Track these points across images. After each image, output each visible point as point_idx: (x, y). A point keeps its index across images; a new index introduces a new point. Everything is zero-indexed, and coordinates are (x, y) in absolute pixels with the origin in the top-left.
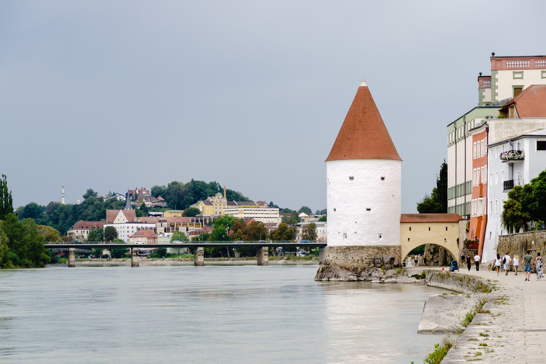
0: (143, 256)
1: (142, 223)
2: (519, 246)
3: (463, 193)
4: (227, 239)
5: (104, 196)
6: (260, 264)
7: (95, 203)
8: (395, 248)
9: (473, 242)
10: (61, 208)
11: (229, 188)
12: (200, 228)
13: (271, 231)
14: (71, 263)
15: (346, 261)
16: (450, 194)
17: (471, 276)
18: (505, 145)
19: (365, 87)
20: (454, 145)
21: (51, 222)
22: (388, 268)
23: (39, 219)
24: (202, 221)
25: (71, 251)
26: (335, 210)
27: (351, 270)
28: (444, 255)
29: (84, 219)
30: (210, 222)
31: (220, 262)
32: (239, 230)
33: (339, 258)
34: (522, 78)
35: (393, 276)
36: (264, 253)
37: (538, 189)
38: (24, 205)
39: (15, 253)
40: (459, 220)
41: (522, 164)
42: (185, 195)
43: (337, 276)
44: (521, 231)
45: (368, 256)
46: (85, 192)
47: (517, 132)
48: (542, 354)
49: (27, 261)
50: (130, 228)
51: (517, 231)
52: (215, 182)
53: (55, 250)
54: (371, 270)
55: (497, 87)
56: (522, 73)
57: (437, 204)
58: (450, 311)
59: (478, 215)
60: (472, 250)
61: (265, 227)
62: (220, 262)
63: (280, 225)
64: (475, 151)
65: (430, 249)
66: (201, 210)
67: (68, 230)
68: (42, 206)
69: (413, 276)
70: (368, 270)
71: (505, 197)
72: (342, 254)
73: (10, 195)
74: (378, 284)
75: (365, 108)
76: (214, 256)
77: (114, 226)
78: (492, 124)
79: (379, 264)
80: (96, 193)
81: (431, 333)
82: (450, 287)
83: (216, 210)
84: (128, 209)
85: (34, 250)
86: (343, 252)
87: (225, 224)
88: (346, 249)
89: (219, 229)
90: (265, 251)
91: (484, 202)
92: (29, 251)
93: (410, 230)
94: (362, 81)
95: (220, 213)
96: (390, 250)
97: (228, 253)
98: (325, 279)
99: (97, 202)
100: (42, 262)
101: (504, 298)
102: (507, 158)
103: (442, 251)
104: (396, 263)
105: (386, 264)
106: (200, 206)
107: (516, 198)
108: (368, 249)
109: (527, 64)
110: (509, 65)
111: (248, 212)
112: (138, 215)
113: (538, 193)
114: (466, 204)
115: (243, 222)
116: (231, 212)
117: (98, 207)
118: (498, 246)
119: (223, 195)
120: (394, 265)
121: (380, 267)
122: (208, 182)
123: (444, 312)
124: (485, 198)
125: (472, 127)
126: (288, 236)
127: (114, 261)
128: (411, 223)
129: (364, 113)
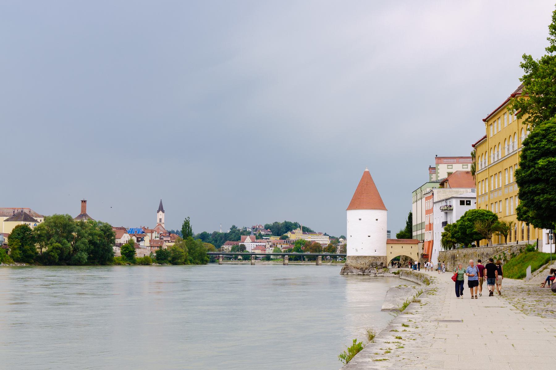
0: (258, 259)
1: (259, 242)
2: (450, 257)
3: (421, 228)
4: (301, 251)
5: (240, 229)
6: (317, 265)
7: (236, 232)
9: (426, 255)
11: (304, 226)
12: (288, 246)
13: (324, 248)
14: (220, 263)
16: (414, 229)
17: (422, 274)
18: (443, 202)
20: (416, 203)
21: (213, 242)
22: (379, 268)
23: (207, 240)
24: (289, 242)
25: (220, 256)
26: (351, 236)
29: (230, 240)
30: (293, 243)
31: (298, 263)
32: (308, 247)
33: (353, 262)
34: (452, 168)
36: (319, 259)
37: (460, 225)
38: (200, 233)
39: (191, 257)
41: (452, 212)
42: (281, 229)
43: (352, 272)
44: (452, 249)
46: (231, 227)
47: (449, 196)
48: (445, 352)
49: (197, 261)
50: (253, 245)
51: (450, 249)
52: (297, 222)
53: (214, 256)
54: (370, 269)
55: (438, 173)
56: (452, 165)
57: (407, 234)
58: (402, 297)
59: (429, 240)
61: (321, 245)
62: (298, 263)
63: (329, 245)
64: (426, 206)
66: (289, 236)
67: (221, 246)
68: (210, 233)
69: (393, 273)
70: (368, 269)
71: (443, 230)
74: (373, 277)
76: (295, 260)
77: (244, 244)
78: (435, 191)
80: (237, 227)
81: (390, 311)
82: (411, 280)
83: (297, 236)
84: (252, 235)
85: (201, 255)
87: (301, 244)
89: (297, 246)
90: (320, 258)
91: (432, 233)
92: (199, 256)
93: (392, 248)
94: (366, 168)
95: (299, 238)
97: (302, 259)
98: (345, 274)
99: (237, 231)
100: (205, 262)
101: (435, 290)
102: (444, 209)
103: (410, 259)
104: (384, 266)
106: (289, 234)
107: (448, 231)
109: (455, 161)
110: (445, 161)
111: (313, 238)
112: (257, 239)
113: (460, 228)
115: (310, 243)
116: (304, 238)
117: (237, 234)
118: (439, 257)
119: (301, 229)
121: (375, 268)
122: (293, 222)
123: (399, 297)
124: (431, 231)
125: (425, 193)
126: (333, 250)
127: (244, 262)
129: (367, 185)
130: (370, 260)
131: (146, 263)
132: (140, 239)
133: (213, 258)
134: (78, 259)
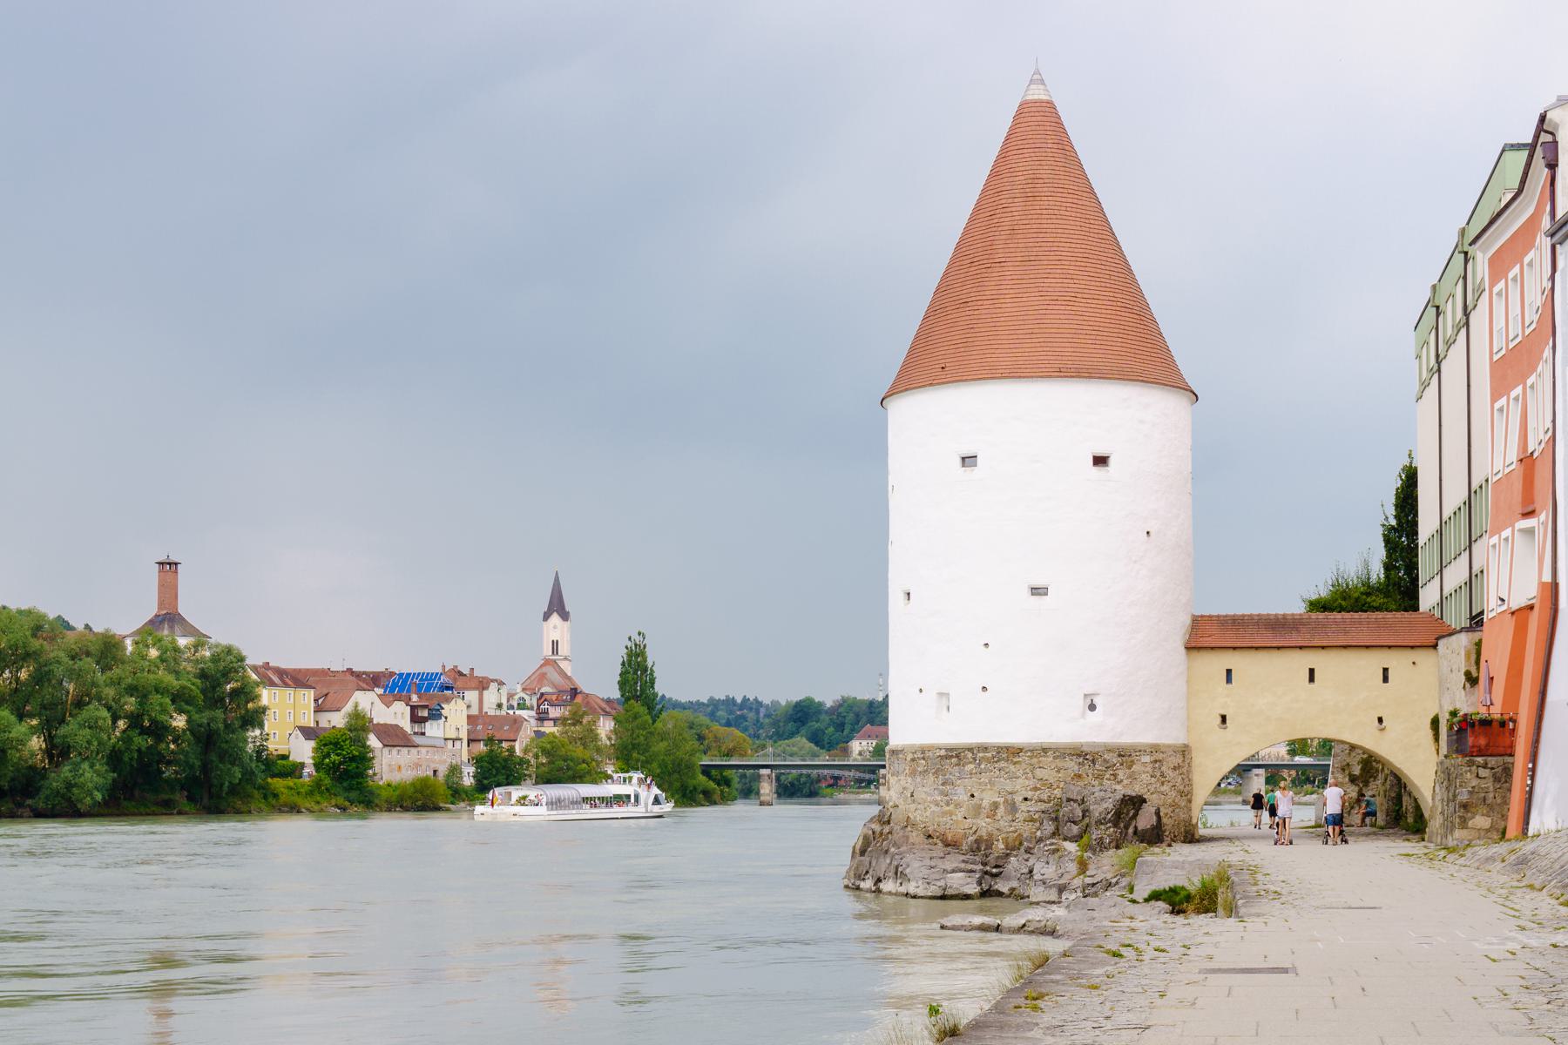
3: (1464, 542)
8: (1160, 756)
9: (1486, 723)
10: (849, 706)
15: (948, 808)
16: (1426, 562)
19: (1042, 102)
22: (1100, 841)
25: (763, 775)
27: (965, 847)
28: (1392, 786)
35: (1114, 881)
40: (1438, 639)
43: (899, 874)
45: (1036, 789)
59: (1517, 602)
60: (1480, 760)
65: (1348, 764)
69: (1155, 896)
72: (932, 778)
73: (651, 670)
75: (1036, 181)
79: (1074, 823)
86: (935, 773)
88: (948, 757)
93: (1229, 680)
96: (1132, 761)
104: (1145, 820)
105: (1099, 823)
108: (1035, 760)
114: (1473, 577)
120: (1136, 827)
128: (1231, 651)
130: (1047, 774)
131: (419, 803)
132: (425, 713)
133: (812, 783)
134: (63, 791)
